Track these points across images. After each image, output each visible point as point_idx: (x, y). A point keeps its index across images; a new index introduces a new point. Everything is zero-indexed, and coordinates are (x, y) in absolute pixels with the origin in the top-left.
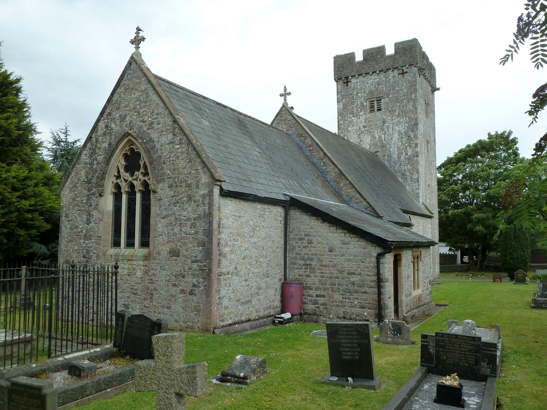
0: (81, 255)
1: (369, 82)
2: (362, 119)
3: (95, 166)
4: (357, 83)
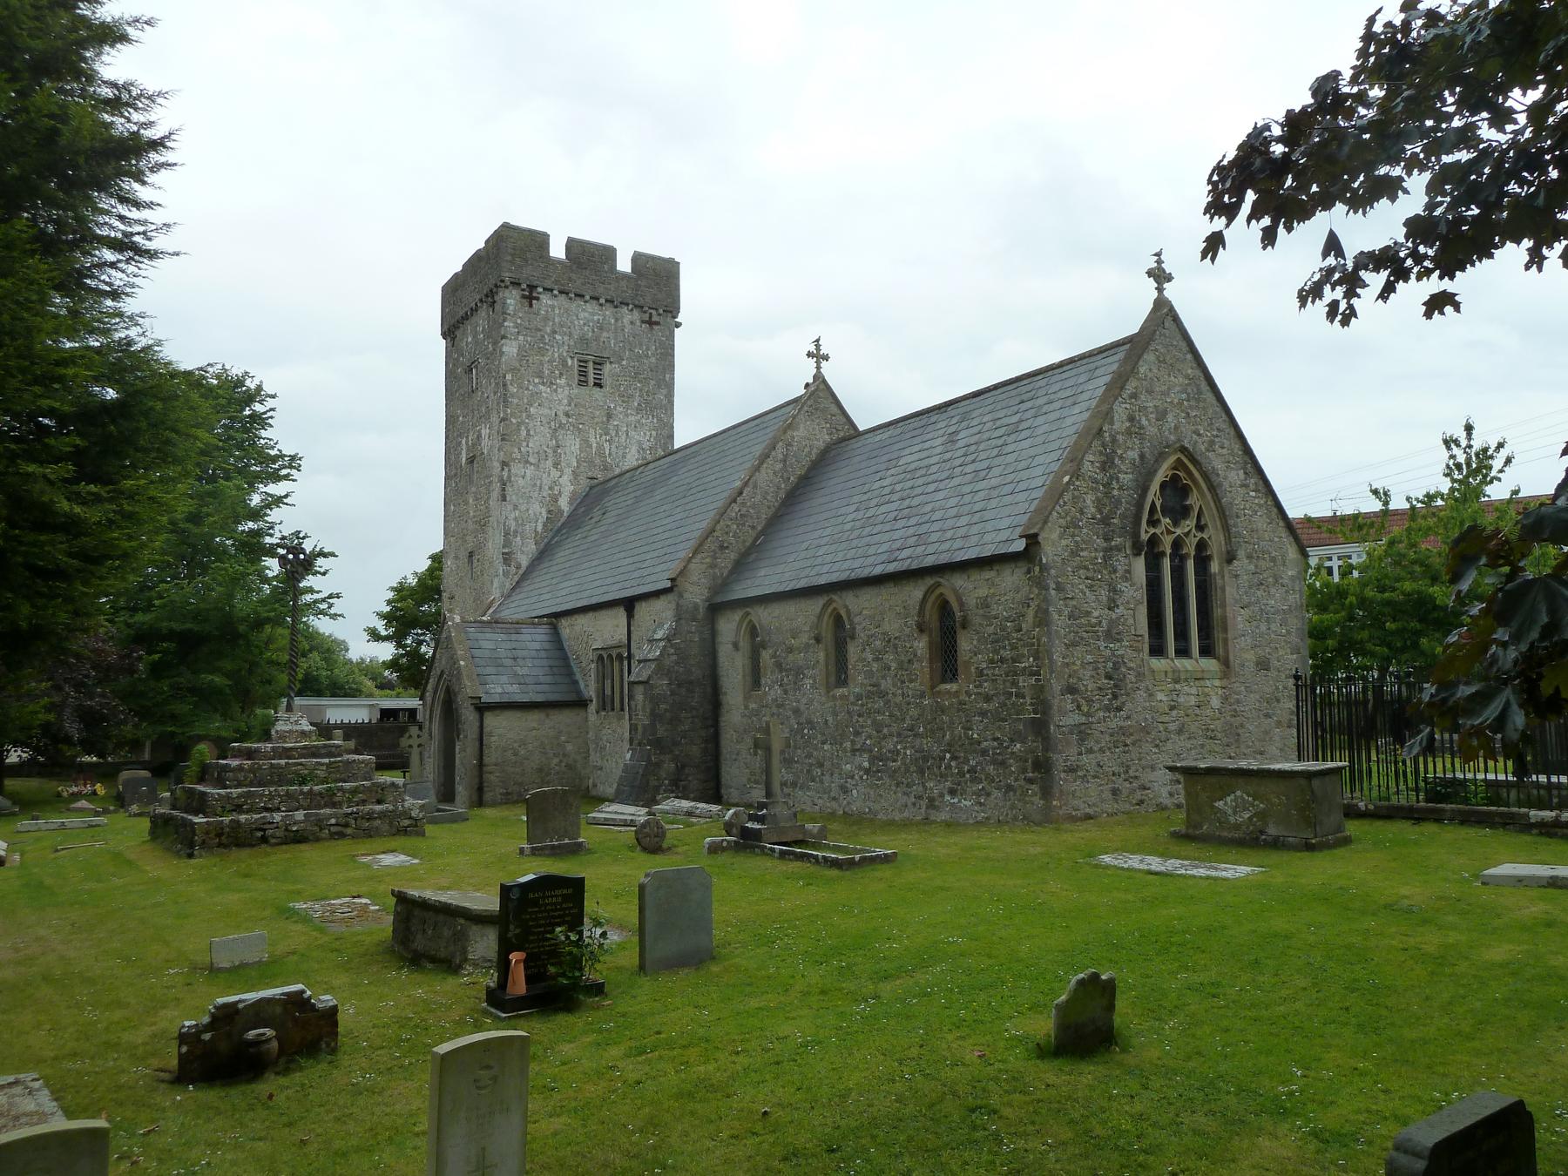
0: (1101, 671)
1: (582, 315)
2: (563, 394)
3: (1115, 492)
4: (553, 307)
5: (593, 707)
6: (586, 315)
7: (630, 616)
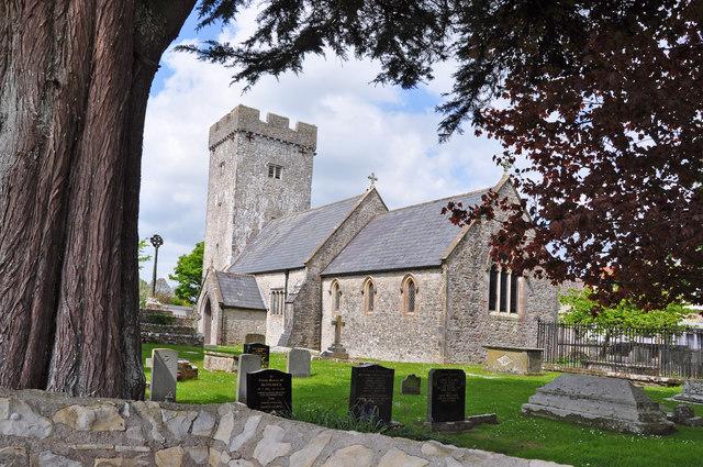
5: (269, 313)
7: (287, 277)
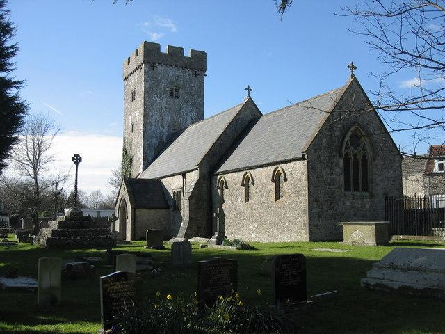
5: (172, 209)
6: (173, 72)
